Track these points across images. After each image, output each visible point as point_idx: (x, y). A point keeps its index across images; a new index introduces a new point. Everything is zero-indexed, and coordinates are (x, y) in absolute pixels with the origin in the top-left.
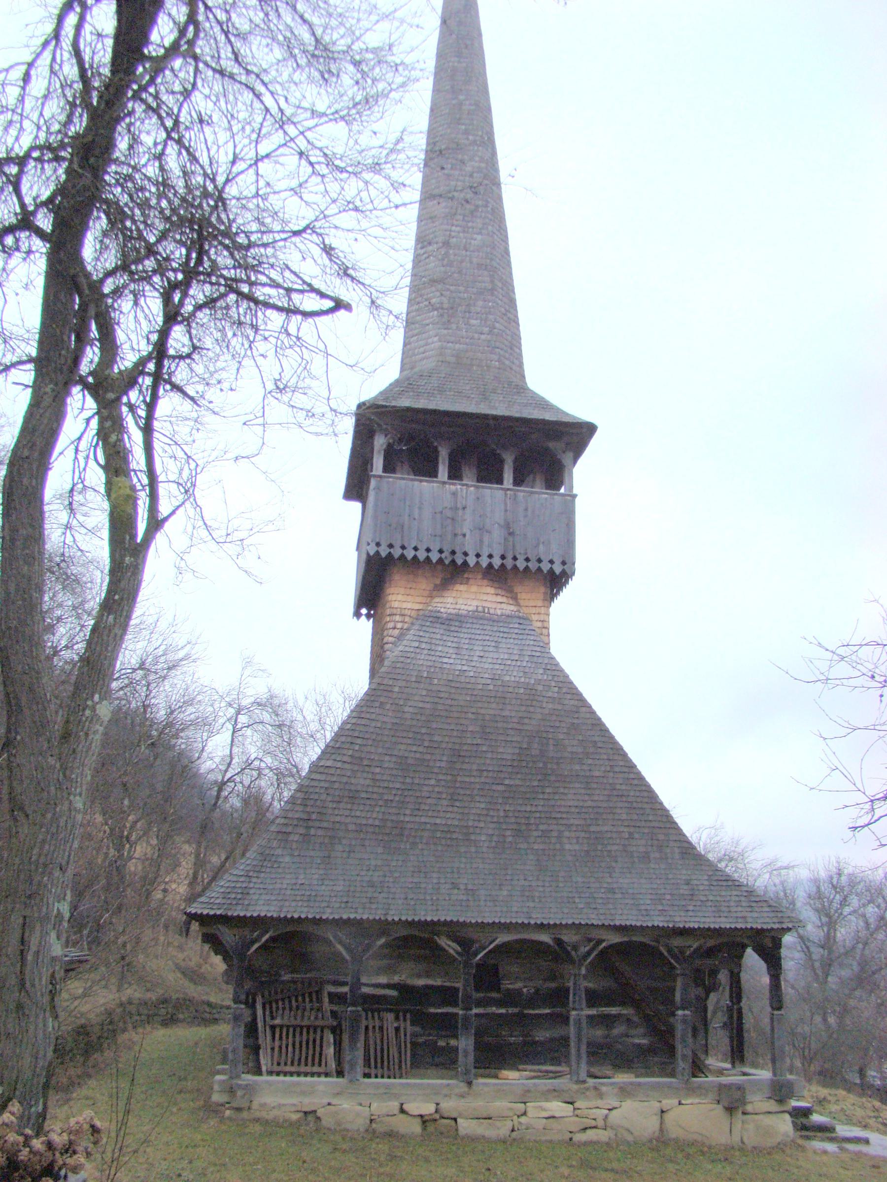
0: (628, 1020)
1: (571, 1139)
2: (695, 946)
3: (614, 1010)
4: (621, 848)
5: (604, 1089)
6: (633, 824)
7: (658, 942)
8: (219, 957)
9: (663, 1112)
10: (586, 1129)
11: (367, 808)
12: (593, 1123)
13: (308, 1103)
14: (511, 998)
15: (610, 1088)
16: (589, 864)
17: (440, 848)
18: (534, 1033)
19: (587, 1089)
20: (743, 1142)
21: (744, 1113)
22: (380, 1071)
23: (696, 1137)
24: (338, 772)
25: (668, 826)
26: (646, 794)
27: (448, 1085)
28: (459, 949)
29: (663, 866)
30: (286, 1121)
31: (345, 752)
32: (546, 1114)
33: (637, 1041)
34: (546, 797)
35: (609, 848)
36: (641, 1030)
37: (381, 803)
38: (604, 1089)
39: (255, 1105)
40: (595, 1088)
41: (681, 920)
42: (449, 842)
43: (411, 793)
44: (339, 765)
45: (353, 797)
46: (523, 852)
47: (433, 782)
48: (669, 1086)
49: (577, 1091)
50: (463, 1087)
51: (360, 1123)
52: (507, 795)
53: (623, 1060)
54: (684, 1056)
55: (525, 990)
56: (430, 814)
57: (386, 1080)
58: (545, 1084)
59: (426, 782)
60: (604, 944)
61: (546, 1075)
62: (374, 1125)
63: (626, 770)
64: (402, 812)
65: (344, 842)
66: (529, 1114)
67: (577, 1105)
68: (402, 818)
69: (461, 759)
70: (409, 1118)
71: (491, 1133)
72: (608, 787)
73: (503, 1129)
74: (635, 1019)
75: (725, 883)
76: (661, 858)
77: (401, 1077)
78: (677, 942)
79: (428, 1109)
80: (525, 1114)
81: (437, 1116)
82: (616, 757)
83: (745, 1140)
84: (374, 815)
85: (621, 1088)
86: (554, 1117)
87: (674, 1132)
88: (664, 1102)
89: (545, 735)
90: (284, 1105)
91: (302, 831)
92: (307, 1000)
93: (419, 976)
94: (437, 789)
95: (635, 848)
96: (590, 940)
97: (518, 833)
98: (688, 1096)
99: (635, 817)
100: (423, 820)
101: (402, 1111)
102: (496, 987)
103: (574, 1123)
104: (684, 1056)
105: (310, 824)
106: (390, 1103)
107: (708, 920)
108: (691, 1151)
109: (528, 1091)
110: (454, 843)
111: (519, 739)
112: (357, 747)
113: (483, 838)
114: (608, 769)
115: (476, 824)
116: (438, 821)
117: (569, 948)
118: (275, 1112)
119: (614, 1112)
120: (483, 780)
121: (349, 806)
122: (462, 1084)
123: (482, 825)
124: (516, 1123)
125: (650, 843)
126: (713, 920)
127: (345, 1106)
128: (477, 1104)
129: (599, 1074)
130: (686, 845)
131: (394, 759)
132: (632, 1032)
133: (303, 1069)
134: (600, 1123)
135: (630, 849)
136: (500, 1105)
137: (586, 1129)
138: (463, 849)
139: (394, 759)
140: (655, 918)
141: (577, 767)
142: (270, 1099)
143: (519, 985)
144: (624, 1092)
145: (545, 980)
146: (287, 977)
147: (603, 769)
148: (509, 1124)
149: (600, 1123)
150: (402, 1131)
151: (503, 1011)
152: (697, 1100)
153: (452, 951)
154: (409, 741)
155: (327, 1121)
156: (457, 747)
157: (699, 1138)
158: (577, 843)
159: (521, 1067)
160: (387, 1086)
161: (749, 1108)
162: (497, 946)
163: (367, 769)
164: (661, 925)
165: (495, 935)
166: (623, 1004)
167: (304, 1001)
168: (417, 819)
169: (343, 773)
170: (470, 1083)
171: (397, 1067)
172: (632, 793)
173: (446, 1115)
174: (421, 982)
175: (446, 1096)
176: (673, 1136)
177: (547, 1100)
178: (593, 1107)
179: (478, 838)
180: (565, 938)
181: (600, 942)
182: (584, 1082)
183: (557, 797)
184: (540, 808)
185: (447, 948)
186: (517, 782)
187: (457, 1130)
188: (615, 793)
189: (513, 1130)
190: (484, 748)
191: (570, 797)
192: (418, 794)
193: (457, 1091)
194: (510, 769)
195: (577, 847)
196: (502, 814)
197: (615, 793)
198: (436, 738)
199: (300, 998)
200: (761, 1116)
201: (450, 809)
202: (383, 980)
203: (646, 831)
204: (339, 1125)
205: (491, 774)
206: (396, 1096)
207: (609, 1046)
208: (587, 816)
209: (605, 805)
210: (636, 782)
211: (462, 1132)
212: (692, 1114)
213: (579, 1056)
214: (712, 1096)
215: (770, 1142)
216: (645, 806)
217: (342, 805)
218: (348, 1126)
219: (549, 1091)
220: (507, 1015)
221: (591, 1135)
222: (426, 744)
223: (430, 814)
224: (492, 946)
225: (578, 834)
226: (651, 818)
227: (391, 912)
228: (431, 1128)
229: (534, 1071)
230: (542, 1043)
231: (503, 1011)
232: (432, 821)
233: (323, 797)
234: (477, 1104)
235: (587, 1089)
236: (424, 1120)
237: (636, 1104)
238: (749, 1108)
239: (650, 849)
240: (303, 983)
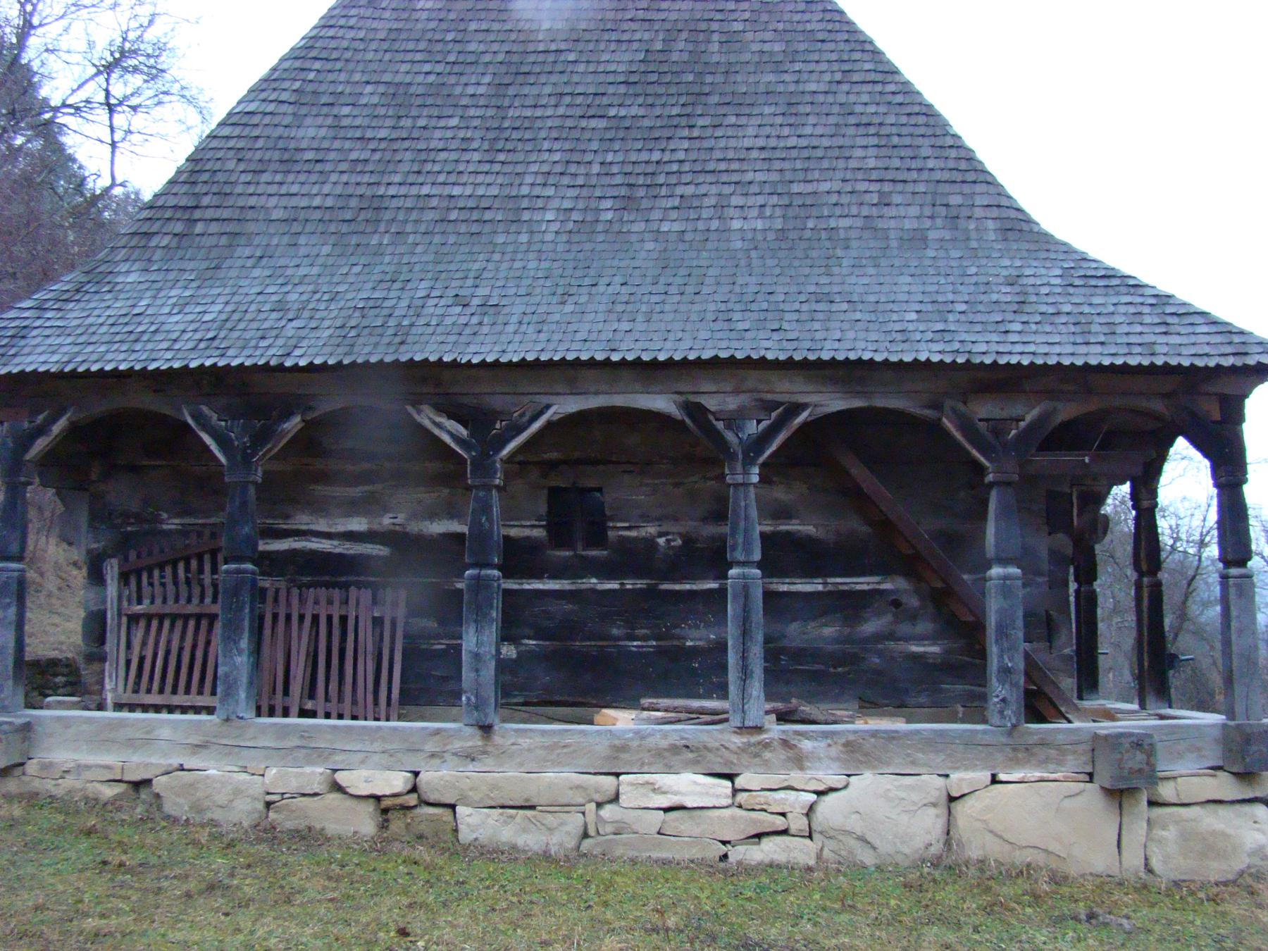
0: (896, 604)
1: (725, 857)
2: (1028, 418)
3: (863, 583)
4: (859, 223)
5: (807, 745)
6: (890, 175)
7: (937, 406)
8: (51, 492)
9: (952, 799)
10: (759, 836)
11: (314, 178)
12: (780, 822)
13: (138, 764)
14: (634, 558)
15: (822, 744)
16: (781, 254)
17: (452, 239)
18: (683, 630)
19: (766, 745)
20: (1150, 871)
21: (1152, 803)
22: (333, 707)
23: (1029, 856)
24: (267, 120)
25: (971, 177)
26: (921, 120)
27: (437, 732)
28: (463, 432)
29: (955, 254)
30: (87, 799)
31: (286, 85)
32: (665, 803)
33: (915, 649)
34: (696, 133)
35: (833, 223)
36: (924, 626)
37: (343, 166)
38: (807, 745)
39: (32, 767)
40: (785, 743)
41: (986, 348)
42: (475, 228)
43: (406, 144)
44: (271, 108)
45: (288, 163)
46: (634, 238)
47: (454, 122)
48: (969, 742)
49: (743, 749)
50: (472, 739)
51: (244, 811)
52: (609, 135)
53: (885, 688)
54: (1005, 672)
55: (661, 541)
56: (441, 178)
57: (347, 722)
58: (665, 735)
59: (442, 123)
60: (803, 416)
61: (694, 716)
62: (272, 815)
63: (879, 77)
64: (386, 180)
65: (257, 241)
66: (622, 798)
67: (739, 782)
68: (381, 191)
69: (520, 79)
70: (350, 803)
71: (532, 840)
72: (836, 109)
73: (560, 834)
74: (914, 602)
75: (1101, 283)
76: (954, 240)
77: (388, 720)
78: (984, 409)
79: (394, 782)
80: (615, 799)
81: (412, 800)
82: (857, 56)
83: (1155, 863)
84: (326, 189)
85: (847, 744)
86: (682, 808)
87: (976, 845)
88: (955, 776)
89: (703, 26)
90: (88, 767)
91: (179, 227)
92: (207, 567)
93: (432, 516)
94: (461, 134)
95: (892, 224)
96: (769, 406)
97: (627, 203)
98: (1015, 763)
99: (896, 163)
100: (425, 190)
101: (337, 788)
102: (597, 536)
103: (733, 823)
104: (1005, 672)
105: (197, 214)
106: (308, 770)
107: (1057, 349)
108: (1007, 891)
109: (623, 748)
110: (487, 228)
111: (646, 36)
112: (311, 76)
113: (550, 216)
114: (838, 77)
115: (537, 191)
116: (456, 191)
117: (720, 425)
118: (69, 782)
119: (832, 797)
120: (561, 111)
121: (278, 178)
122: (469, 730)
123: (550, 191)
124: (591, 818)
125: (927, 211)
126: (1069, 349)
127: (212, 772)
128: (509, 777)
129: (822, 718)
130: (1013, 214)
131: (382, 89)
132: (905, 628)
133: (179, 699)
134: (797, 823)
135: (881, 224)
136: (558, 779)
137: (759, 836)
138: (501, 239)
139: (382, 89)
140: (923, 346)
141: (771, 77)
142: (62, 756)
143: (652, 530)
144: (857, 755)
145: (704, 520)
146: (172, 524)
147: (827, 77)
148: (574, 822)
149: (797, 823)
150: (332, 828)
151: (613, 585)
152: (900, 725)
153: (446, 438)
154: (419, 57)
155: (175, 805)
156: (515, 58)
157: (1040, 859)
158: (761, 216)
159: (645, 702)
160: (303, 733)
161: (1166, 791)
162: (549, 425)
163: (325, 110)
164: (935, 358)
165: (545, 400)
166: (884, 570)
167: (201, 570)
168: (414, 190)
169: (276, 120)
170: (486, 729)
171: (370, 698)
172: (891, 119)
173: (433, 797)
174: (438, 527)
175: (433, 756)
176: (974, 853)
177: (670, 770)
178: (778, 787)
179: (537, 216)
180: (711, 403)
181: (797, 408)
182: (758, 729)
183: (719, 133)
184: (681, 155)
185: (436, 431)
186: (634, 111)
187: (456, 831)
188: (852, 120)
189: (586, 835)
190: (572, 57)
191: (751, 131)
192: (422, 145)
193: (457, 745)
194: (622, 89)
195: (759, 225)
196: (596, 169)
197: (852, 120)
198: (472, 47)
199: (194, 563)
200: (1196, 809)
201: (486, 167)
202: (358, 524)
203: (921, 188)
204: (200, 811)
205: (579, 100)
206: (318, 754)
207: (851, 659)
208: (787, 165)
209: (826, 142)
210: (899, 99)
211: (465, 835)
212: (1028, 805)
213: (745, 672)
214: (1075, 763)
215: (1216, 870)
216: (920, 141)
217: (265, 177)
218: (217, 815)
219: (674, 749)
220: (622, 592)
221: (770, 850)
222: (452, 58)
223: (441, 178)
224: (536, 426)
225: (760, 200)
226: (931, 164)
227: (298, 352)
228: (397, 824)
229: (675, 710)
230: (695, 651)
231: (613, 585)
232: (447, 191)
233: (231, 165)
234: (509, 777)
235: (766, 745)
236: (384, 807)
237: (888, 782)
238: (1166, 791)
239: (928, 223)
240: (200, 534)
